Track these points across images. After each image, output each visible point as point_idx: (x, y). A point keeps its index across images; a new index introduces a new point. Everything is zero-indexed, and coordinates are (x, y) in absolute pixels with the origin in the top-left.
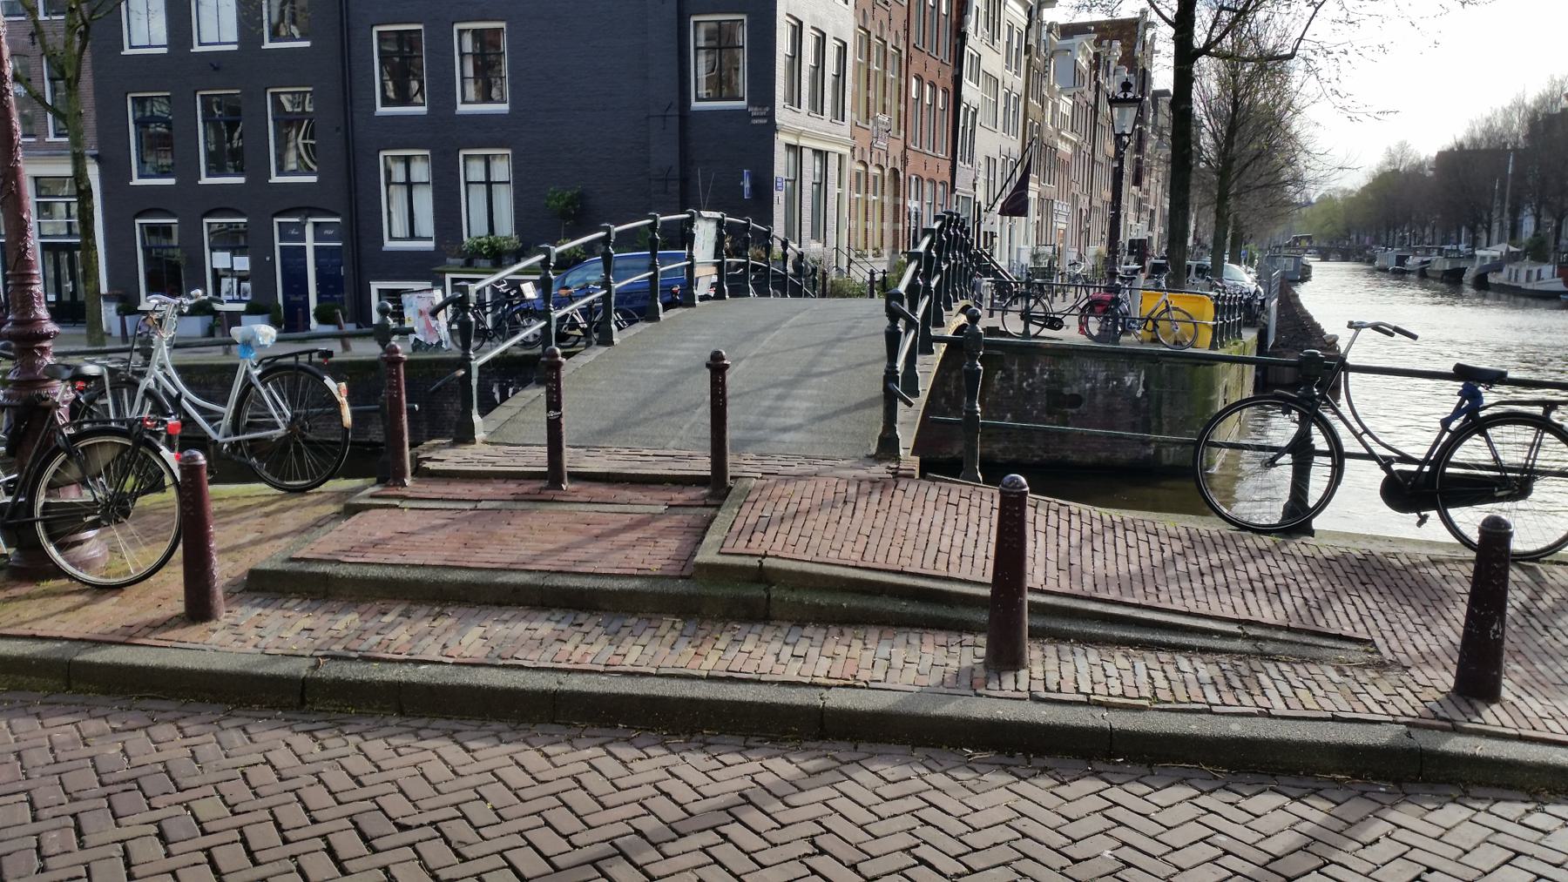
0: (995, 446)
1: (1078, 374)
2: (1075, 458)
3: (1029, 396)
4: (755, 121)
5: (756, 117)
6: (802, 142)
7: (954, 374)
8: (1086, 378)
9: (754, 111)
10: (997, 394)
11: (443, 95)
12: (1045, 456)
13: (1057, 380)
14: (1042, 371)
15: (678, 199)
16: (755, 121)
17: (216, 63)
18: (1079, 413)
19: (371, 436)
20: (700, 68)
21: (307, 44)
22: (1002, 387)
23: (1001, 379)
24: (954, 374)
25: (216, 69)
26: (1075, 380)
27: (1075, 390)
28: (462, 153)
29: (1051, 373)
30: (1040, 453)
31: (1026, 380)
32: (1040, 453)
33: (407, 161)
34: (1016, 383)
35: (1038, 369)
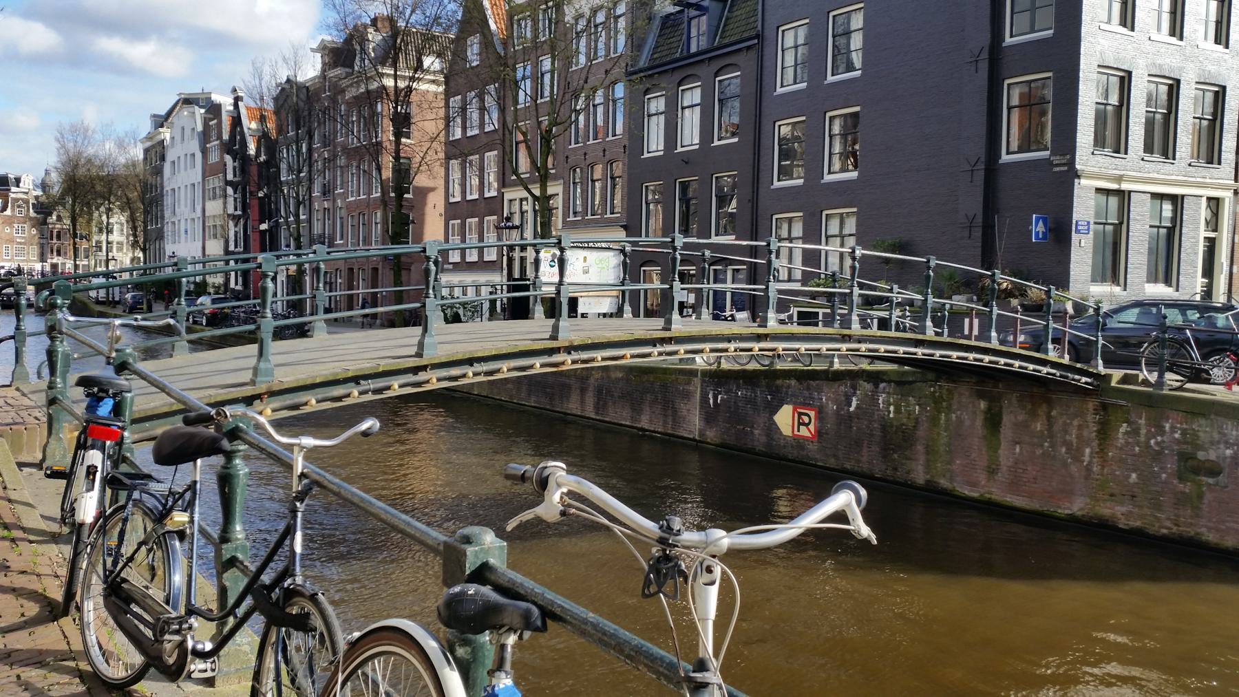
0: (1118, 508)
1: (1216, 436)
2: (1211, 537)
3: (1157, 456)
4: (1058, 169)
5: (1057, 165)
6: (1125, 186)
7: (1076, 423)
8: (1226, 442)
9: (1056, 160)
10: (1121, 449)
11: (814, 171)
12: (1175, 529)
13: (1190, 439)
14: (1173, 429)
15: (980, 244)
16: (1058, 169)
17: (687, 160)
18: (1217, 484)
19: (642, 423)
20: (1012, 128)
21: (736, 140)
22: (1127, 443)
23: (1127, 433)
24: (1076, 423)
25: (686, 163)
26: (1212, 443)
27: (1212, 455)
28: (825, 213)
29: (1184, 433)
30: (1168, 524)
31: (1154, 437)
32: (1168, 524)
33: (790, 220)
34: (1142, 439)
35: (1167, 426)
